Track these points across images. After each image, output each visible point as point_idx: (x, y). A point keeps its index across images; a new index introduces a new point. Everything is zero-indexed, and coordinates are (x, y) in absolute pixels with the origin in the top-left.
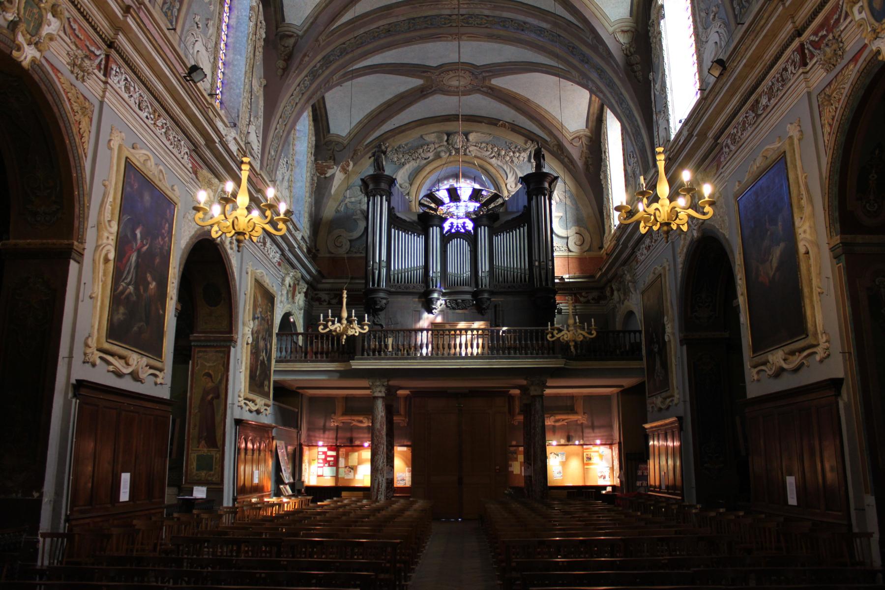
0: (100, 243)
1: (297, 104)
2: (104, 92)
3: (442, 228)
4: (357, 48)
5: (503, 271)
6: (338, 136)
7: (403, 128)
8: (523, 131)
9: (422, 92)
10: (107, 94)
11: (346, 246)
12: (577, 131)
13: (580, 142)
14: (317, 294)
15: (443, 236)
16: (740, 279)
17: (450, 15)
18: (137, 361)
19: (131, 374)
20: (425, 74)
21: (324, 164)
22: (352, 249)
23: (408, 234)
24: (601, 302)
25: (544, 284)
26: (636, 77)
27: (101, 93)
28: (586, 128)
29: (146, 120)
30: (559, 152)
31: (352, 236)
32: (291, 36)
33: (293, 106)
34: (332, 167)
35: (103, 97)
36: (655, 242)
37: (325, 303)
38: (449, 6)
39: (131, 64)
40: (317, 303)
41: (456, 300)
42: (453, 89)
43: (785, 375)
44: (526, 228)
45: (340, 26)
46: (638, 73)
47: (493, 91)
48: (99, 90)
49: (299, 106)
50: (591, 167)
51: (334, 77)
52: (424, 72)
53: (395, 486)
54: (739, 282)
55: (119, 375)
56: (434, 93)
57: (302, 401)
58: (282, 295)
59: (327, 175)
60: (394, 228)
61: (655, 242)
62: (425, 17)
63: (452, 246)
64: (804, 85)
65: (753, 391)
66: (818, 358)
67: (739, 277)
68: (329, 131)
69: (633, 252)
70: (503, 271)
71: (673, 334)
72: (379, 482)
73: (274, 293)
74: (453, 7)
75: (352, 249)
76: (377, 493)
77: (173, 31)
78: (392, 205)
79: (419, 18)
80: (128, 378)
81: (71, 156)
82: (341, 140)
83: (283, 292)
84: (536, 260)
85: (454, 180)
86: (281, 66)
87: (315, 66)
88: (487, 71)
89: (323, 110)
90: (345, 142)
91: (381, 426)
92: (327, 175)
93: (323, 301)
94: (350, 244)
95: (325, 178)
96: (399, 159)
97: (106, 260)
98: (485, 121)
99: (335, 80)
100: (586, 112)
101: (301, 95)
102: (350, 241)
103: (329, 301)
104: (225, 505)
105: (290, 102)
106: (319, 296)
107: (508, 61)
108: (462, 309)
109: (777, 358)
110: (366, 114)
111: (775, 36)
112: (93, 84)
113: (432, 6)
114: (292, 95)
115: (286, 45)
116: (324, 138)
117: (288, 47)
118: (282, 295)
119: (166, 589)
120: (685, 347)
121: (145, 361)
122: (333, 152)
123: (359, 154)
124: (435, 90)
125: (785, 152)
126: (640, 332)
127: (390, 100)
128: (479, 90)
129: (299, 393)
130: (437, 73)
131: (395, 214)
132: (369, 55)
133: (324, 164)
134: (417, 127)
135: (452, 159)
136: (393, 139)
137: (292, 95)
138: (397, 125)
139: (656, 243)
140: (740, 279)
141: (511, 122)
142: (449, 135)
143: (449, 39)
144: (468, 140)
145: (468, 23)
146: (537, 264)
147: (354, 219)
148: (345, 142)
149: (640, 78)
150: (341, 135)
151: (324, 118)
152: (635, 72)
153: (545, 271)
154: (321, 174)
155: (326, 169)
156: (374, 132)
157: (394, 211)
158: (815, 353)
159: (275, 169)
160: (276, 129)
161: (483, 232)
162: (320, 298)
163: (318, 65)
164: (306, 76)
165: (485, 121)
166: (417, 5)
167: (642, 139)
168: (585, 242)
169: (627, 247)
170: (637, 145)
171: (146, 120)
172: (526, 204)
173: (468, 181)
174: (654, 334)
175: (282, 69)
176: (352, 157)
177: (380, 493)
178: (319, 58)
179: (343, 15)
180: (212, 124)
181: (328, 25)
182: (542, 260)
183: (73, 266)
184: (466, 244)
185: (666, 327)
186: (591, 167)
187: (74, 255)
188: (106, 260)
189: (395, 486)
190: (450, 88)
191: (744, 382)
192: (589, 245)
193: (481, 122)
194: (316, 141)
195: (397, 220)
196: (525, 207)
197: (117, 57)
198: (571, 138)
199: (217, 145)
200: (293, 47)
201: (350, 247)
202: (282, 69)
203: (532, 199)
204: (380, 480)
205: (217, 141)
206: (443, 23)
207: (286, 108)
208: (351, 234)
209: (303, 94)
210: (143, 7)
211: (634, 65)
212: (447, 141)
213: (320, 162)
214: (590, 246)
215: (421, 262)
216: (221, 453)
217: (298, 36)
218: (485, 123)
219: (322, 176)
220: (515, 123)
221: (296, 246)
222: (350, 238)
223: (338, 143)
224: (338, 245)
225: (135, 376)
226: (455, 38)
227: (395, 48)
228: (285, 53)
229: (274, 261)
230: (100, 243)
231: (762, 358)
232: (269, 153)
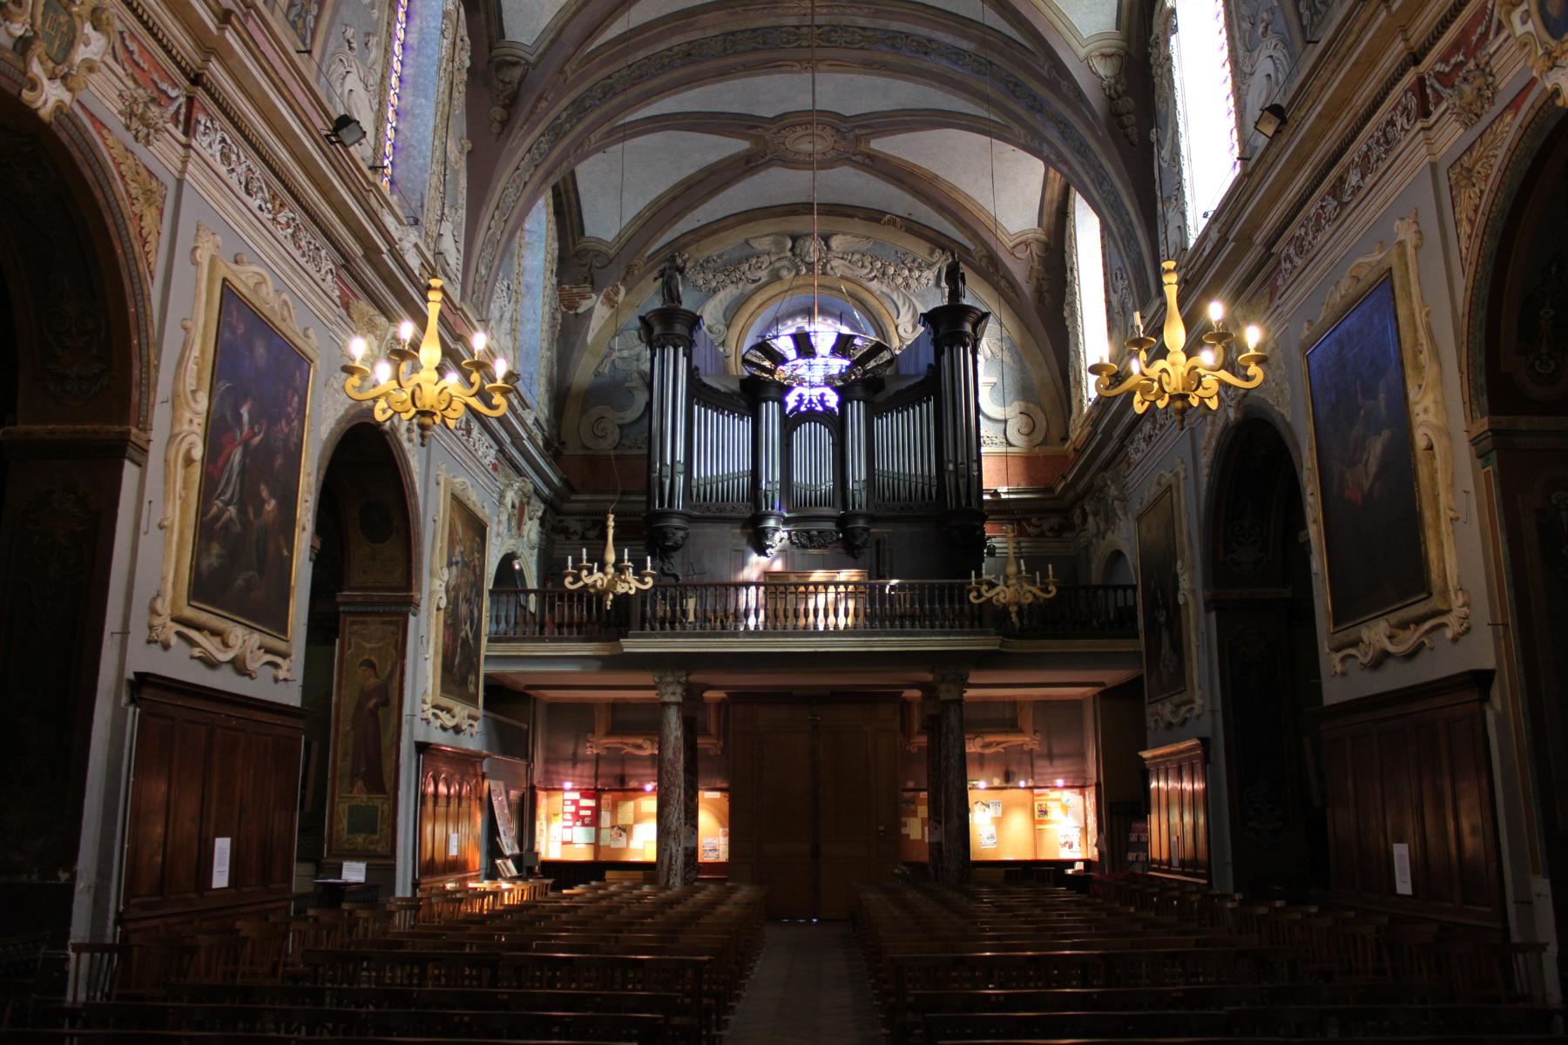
0: (177, 430)
1: (525, 183)
2: (185, 163)
3: (783, 404)
4: (633, 85)
5: (891, 481)
6: (599, 240)
7: (715, 227)
8: (926, 232)
9: (748, 162)
10: (190, 167)
11: (614, 436)
12: (1023, 233)
13: (1028, 252)
14: (561, 521)
15: (784, 418)
16: (1312, 494)
17: (798, 27)
18: (243, 639)
19: (232, 662)
20: (752, 132)
21: (575, 290)
22: (623, 442)
23: (723, 414)
24: (1064, 536)
25: (963, 502)
26: (1126, 136)
27: (179, 165)
28: (1039, 226)
29: (258, 212)
30: (991, 270)
31: (623, 418)
32: (515, 64)
33: (518, 187)
34: (588, 295)
35: (183, 171)
36: (1160, 429)
37: (576, 538)
38: (796, 10)
39: (232, 114)
40: (562, 537)
41: (808, 532)
42: (802, 158)
43: (1391, 665)
44: (931, 404)
45: (602, 45)
46: (1130, 130)
47: (873, 161)
48: (176, 160)
49: (530, 187)
50: (1047, 296)
51: (592, 136)
52: (752, 127)
53: (700, 860)
54: (1310, 499)
55: (211, 664)
56: (769, 164)
57: (534, 710)
58: (499, 522)
59: (580, 310)
60: (698, 404)
61: (1160, 429)
62: (754, 30)
63: (801, 435)
64: (1424, 150)
65: (1333, 693)
66: (1449, 633)
67: (1309, 491)
68: (582, 232)
69: (1122, 446)
70: (891, 481)
71: (1193, 591)
72: (671, 853)
73: (486, 520)
74: (803, 12)
75: (623, 442)
76: (669, 874)
77: (306, 55)
78: (695, 362)
79: (743, 31)
80: (228, 670)
81: (125, 276)
82: (604, 248)
83: (501, 518)
84: (949, 461)
85: (804, 318)
86: (498, 118)
87: (558, 117)
88: (862, 127)
89: (572, 196)
90: (612, 252)
91: (674, 754)
92: (580, 310)
93: (572, 534)
94: (621, 433)
95: (577, 314)
96: (706, 282)
97: (189, 461)
98: (859, 214)
99: (593, 141)
100: (1039, 198)
101: (533, 168)
102: (621, 427)
103: (583, 533)
104: (399, 894)
105: (514, 181)
106: (565, 524)
107: (900, 108)
108: (819, 547)
109: (1376, 633)
110: (648, 202)
111: (1373, 63)
112: (165, 149)
113: (766, 11)
114: (518, 168)
115: (507, 80)
116: (574, 245)
117: (510, 83)
118: (499, 522)
119: (293, 1043)
120: (1213, 615)
121: (256, 639)
122: (589, 270)
123: (636, 272)
124: (771, 160)
125: (1390, 269)
126: (1134, 588)
127: (691, 177)
128: (848, 159)
129: (529, 696)
130: (775, 130)
131: (700, 380)
132: (654, 98)
133: (575, 290)
134: (739, 225)
135: (800, 281)
136: (695, 245)
137: (518, 168)
138: (704, 222)
139: (1163, 431)
140: (1312, 494)
141: (906, 215)
142: (795, 239)
143: (795, 69)
144: (829, 248)
145: (828, 41)
146: (951, 467)
147: (627, 388)
148: (611, 252)
149: (1135, 138)
150: (605, 238)
151: (574, 210)
152: (1126, 127)
153: (966, 480)
154: (569, 308)
155: (577, 299)
156: (663, 234)
157: (698, 374)
158: (1444, 625)
159: (487, 299)
160: (489, 228)
161: (856, 411)
162: (568, 528)
163: (564, 115)
164: (543, 135)
165: (859, 214)
166: (738, 9)
167: (1138, 245)
168: (1036, 429)
169: (1111, 437)
170: (1128, 256)
171: (258, 212)
172: (932, 361)
173: (830, 321)
174: (1159, 592)
175: (500, 122)
176: (624, 279)
177: (673, 873)
178: (565, 102)
179: (607, 27)
180: (376, 220)
181: (581, 45)
182: (960, 461)
183: (130, 471)
184: (825, 432)
185: (1181, 579)
186: (1047, 296)
187: (131, 451)
188: (189, 461)
189: (700, 860)
190: (797, 157)
191: (1318, 676)
192: (1043, 434)
193: (852, 216)
194: (560, 249)
195: (704, 389)
196: (930, 366)
197: (207, 100)
198: (1011, 244)
199: (385, 256)
200: (520, 83)
201: (621, 438)
202: (500, 122)
203: (943, 353)
204: (674, 850)
205: (385, 250)
206: (785, 40)
207: (506, 192)
208: (621, 414)
209: (536, 166)
210: (253, 12)
211: (1123, 115)
212: (792, 249)
213: (567, 287)
214: (1046, 436)
215: (746, 465)
216: (391, 802)
217: (527, 63)
218: (860, 218)
219: (571, 312)
220: (913, 218)
221: (524, 435)
222: (620, 422)
223: (598, 254)
224: (599, 433)
225: (239, 666)
226: (806, 68)
227: (700, 86)
228: (505, 94)
229: (486, 462)
230: (177, 430)
231: (1350, 635)
232: (477, 271)
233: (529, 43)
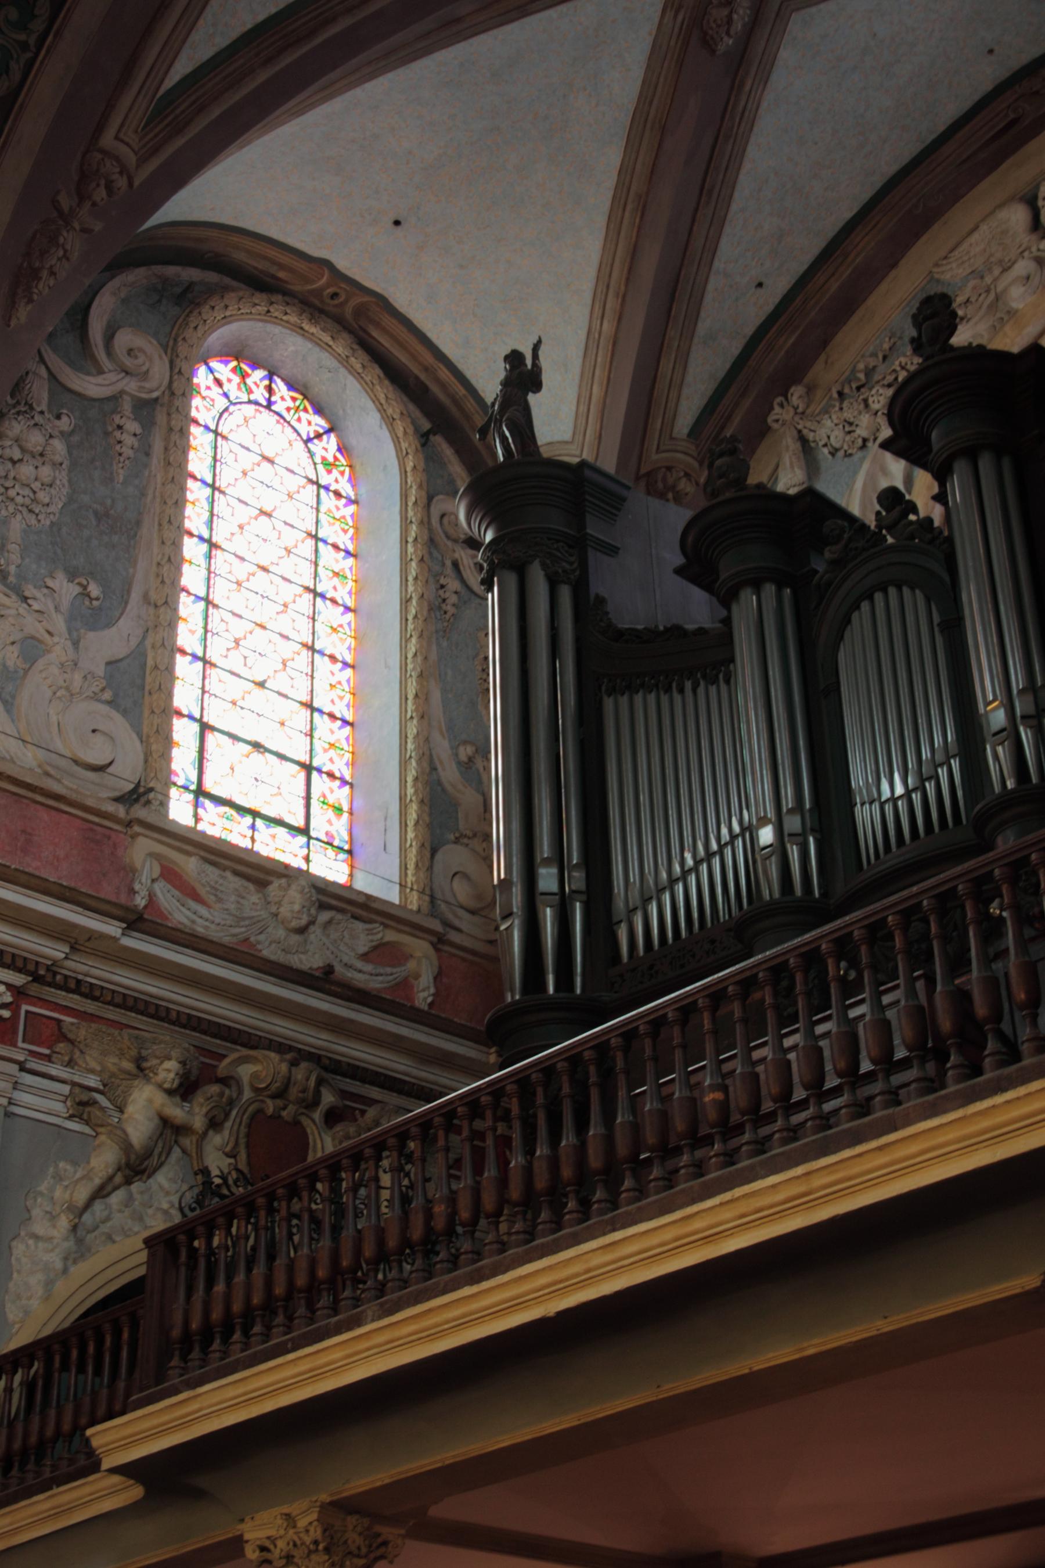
9: (708, 43)
89: (444, 374)
127: (625, 171)
138: (779, 286)
150: (557, 438)
184: (915, 600)
233: (568, 437)
